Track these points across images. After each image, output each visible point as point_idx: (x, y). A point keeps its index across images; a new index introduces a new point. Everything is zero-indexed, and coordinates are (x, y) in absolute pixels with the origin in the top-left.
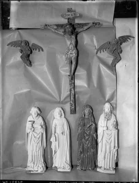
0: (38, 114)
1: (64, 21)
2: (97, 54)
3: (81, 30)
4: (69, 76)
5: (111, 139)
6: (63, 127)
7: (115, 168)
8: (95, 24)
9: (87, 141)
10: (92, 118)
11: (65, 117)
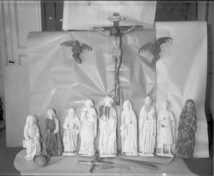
0: (91, 106)
1: (111, 24)
2: (139, 53)
3: (126, 32)
4: (115, 72)
5: (150, 127)
6: (131, 117)
7: (153, 152)
8: (137, 27)
9: (185, 132)
10: (194, 112)
11: (132, 109)
